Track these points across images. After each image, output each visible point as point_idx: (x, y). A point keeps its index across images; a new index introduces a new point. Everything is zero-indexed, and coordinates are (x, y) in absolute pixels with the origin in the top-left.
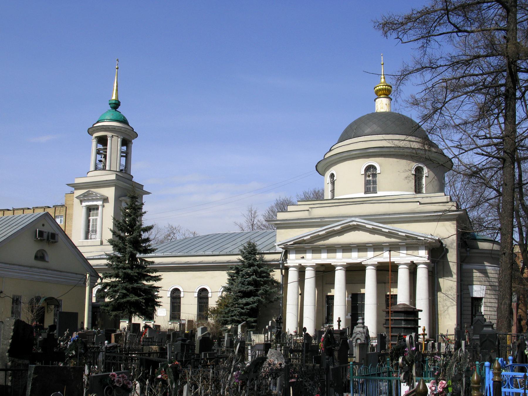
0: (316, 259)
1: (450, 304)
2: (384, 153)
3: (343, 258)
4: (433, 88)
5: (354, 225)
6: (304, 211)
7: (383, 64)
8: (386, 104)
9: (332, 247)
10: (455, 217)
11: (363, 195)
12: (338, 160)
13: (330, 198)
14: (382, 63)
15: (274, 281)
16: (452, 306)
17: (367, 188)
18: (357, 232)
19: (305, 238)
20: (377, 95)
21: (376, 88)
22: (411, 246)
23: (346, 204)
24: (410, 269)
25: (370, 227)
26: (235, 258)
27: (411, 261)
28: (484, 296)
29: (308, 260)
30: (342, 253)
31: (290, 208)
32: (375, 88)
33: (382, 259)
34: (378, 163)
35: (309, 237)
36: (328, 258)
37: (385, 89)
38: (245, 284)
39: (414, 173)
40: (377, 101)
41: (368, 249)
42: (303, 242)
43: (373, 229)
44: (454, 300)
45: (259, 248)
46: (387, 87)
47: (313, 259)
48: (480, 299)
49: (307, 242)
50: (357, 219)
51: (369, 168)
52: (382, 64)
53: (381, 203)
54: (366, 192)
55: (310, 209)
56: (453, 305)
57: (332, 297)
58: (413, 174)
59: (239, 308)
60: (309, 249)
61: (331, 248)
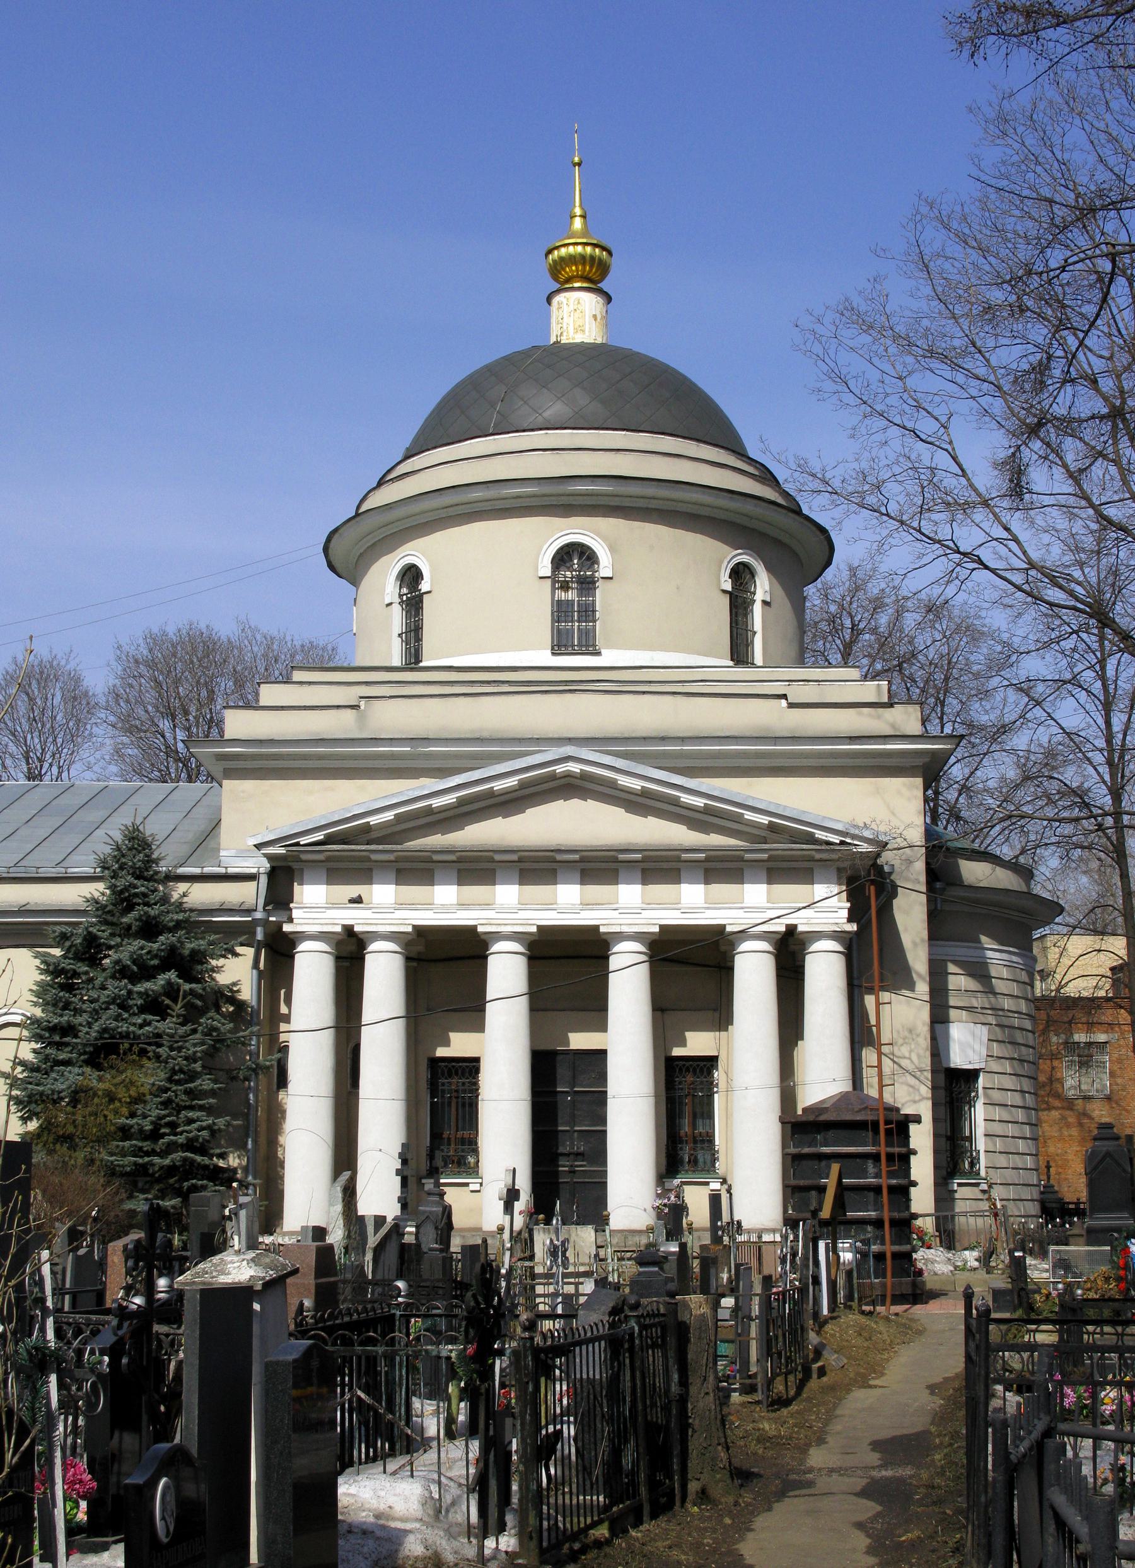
0: (662, 905)
1: (909, 1094)
2: (626, 503)
3: (523, 905)
4: (1064, 271)
5: (568, 775)
6: (338, 707)
7: (579, 164)
8: (595, 317)
9: (667, 860)
10: (919, 762)
11: (545, 658)
12: (443, 514)
13: (397, 661)
14: (576, 159)
15: (227, 996)
16: (915, 1102)
17: (559, 631)
18: (575, 803)
19: (374, 820)
20: (556, 279)
21: (556, 252)
22: (785, 865)
23: (496, 689)
24: (339, 959)
25: (636, 784)
26: (71, 895)
27: (344, 926)
28: (982, 1066)
29: (379, 909)
30: (455, 887)
31: (269, 694)
32: (550, 252)
33: (677, 914)
34: (605, 539)
35: (389, 816)
36: (462, 905)
37: (592, 258)
38: (131, 1007)
39: (728, 586)
40: (556, 300)
41: (622, 875)
42: (364, 834)
43: (645, 793)
44: (922, 1078)
45: (167, 858)
46: (597, 250)
47: (400, 905)
48: (971, 1076)
49: (374, 835)
50: (569, 750)
51: (568, 553)
52: (575, 165)
53: (644, 693)
54: (560, 645)
55: (362, 704)
56: (917, 1098)
57: (470, 1067)
58: (724, 592)
59: (199, 1114)
60: (384, 865)
61: (473, 866)
